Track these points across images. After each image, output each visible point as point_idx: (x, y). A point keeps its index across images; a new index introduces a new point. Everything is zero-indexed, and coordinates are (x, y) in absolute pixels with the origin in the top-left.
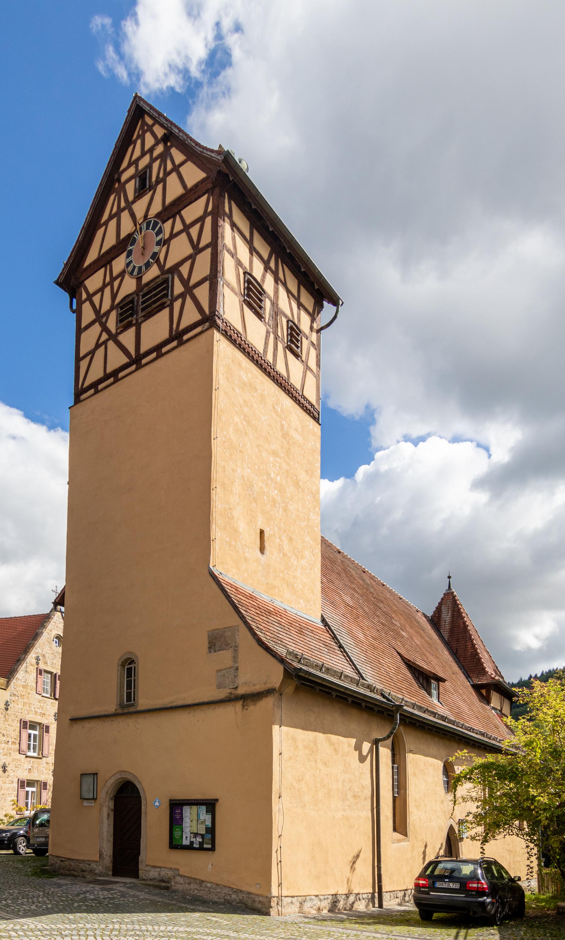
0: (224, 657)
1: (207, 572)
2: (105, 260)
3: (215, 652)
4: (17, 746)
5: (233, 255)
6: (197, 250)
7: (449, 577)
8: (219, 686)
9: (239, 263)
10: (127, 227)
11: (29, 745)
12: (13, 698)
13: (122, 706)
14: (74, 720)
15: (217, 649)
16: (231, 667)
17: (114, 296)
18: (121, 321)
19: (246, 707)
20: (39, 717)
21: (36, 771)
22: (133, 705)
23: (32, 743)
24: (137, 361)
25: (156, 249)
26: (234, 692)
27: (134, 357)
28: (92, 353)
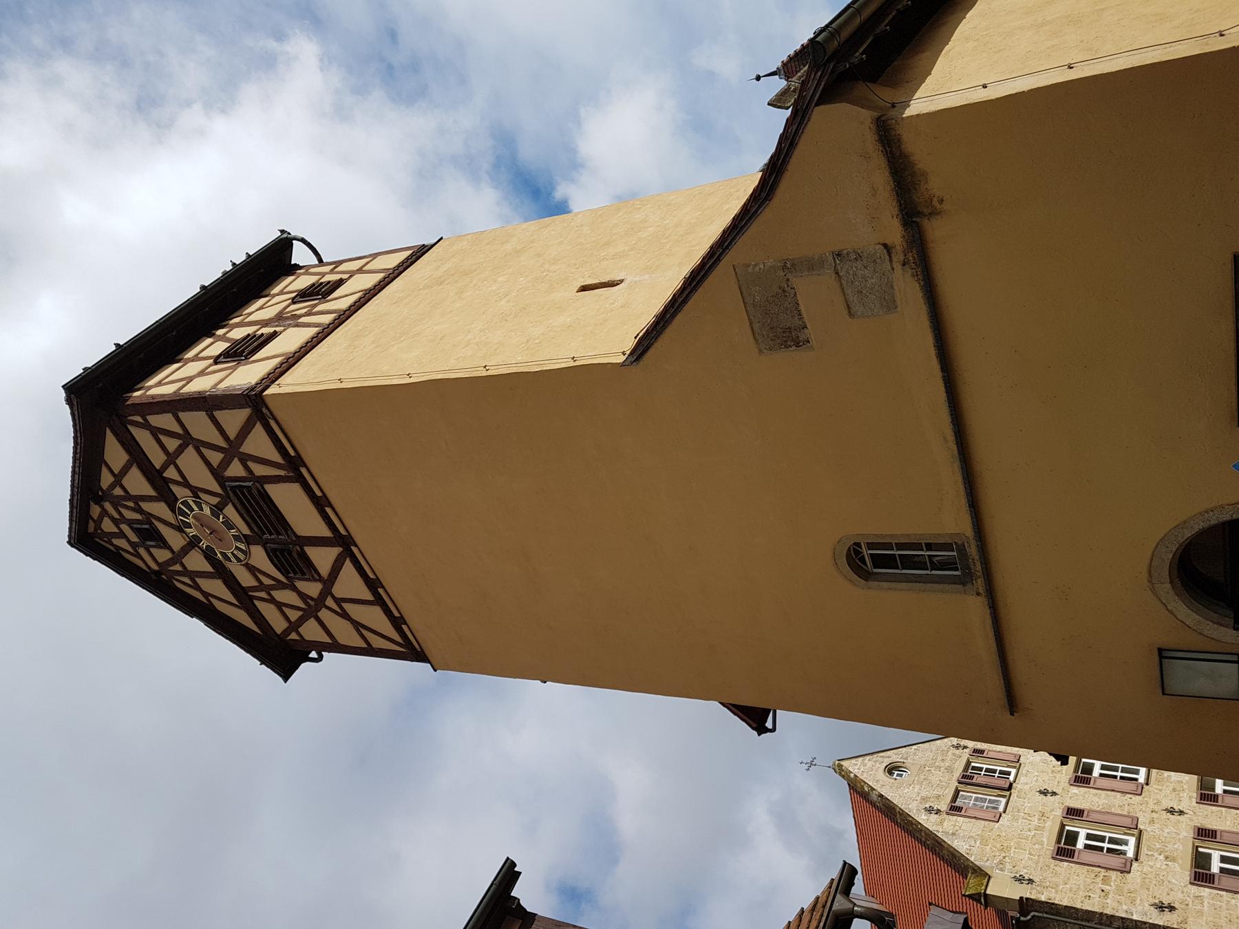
0: (815, 297)
1: (634, 368)
2: (244, 597)
3: (805, 327)
4: (1113, 875)
5: (190, 379)
6: (187, 439)
7: (758, 78)
8: (890, 305)
9: (202, 373)
10: (195, 561)
11: (1102, 839)
12: (1008, 866)
13: (966, 579)
14: (1012, 703)
15: (798, 323)
16: (837, 273)
17: (280, 586)
18: (304, 574)
19: (935, 202)
20: (1049, 823)
21: (1170, 846)
22: (962, 549)
23: (1106, 845)
24: (344, 542)
25: (207, 511)
26: (898, 257)
27: (108, 432)
28: (358, 626)
